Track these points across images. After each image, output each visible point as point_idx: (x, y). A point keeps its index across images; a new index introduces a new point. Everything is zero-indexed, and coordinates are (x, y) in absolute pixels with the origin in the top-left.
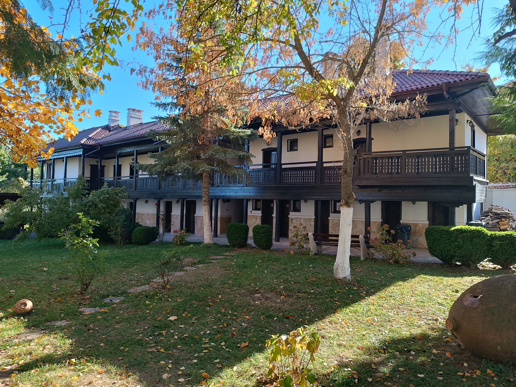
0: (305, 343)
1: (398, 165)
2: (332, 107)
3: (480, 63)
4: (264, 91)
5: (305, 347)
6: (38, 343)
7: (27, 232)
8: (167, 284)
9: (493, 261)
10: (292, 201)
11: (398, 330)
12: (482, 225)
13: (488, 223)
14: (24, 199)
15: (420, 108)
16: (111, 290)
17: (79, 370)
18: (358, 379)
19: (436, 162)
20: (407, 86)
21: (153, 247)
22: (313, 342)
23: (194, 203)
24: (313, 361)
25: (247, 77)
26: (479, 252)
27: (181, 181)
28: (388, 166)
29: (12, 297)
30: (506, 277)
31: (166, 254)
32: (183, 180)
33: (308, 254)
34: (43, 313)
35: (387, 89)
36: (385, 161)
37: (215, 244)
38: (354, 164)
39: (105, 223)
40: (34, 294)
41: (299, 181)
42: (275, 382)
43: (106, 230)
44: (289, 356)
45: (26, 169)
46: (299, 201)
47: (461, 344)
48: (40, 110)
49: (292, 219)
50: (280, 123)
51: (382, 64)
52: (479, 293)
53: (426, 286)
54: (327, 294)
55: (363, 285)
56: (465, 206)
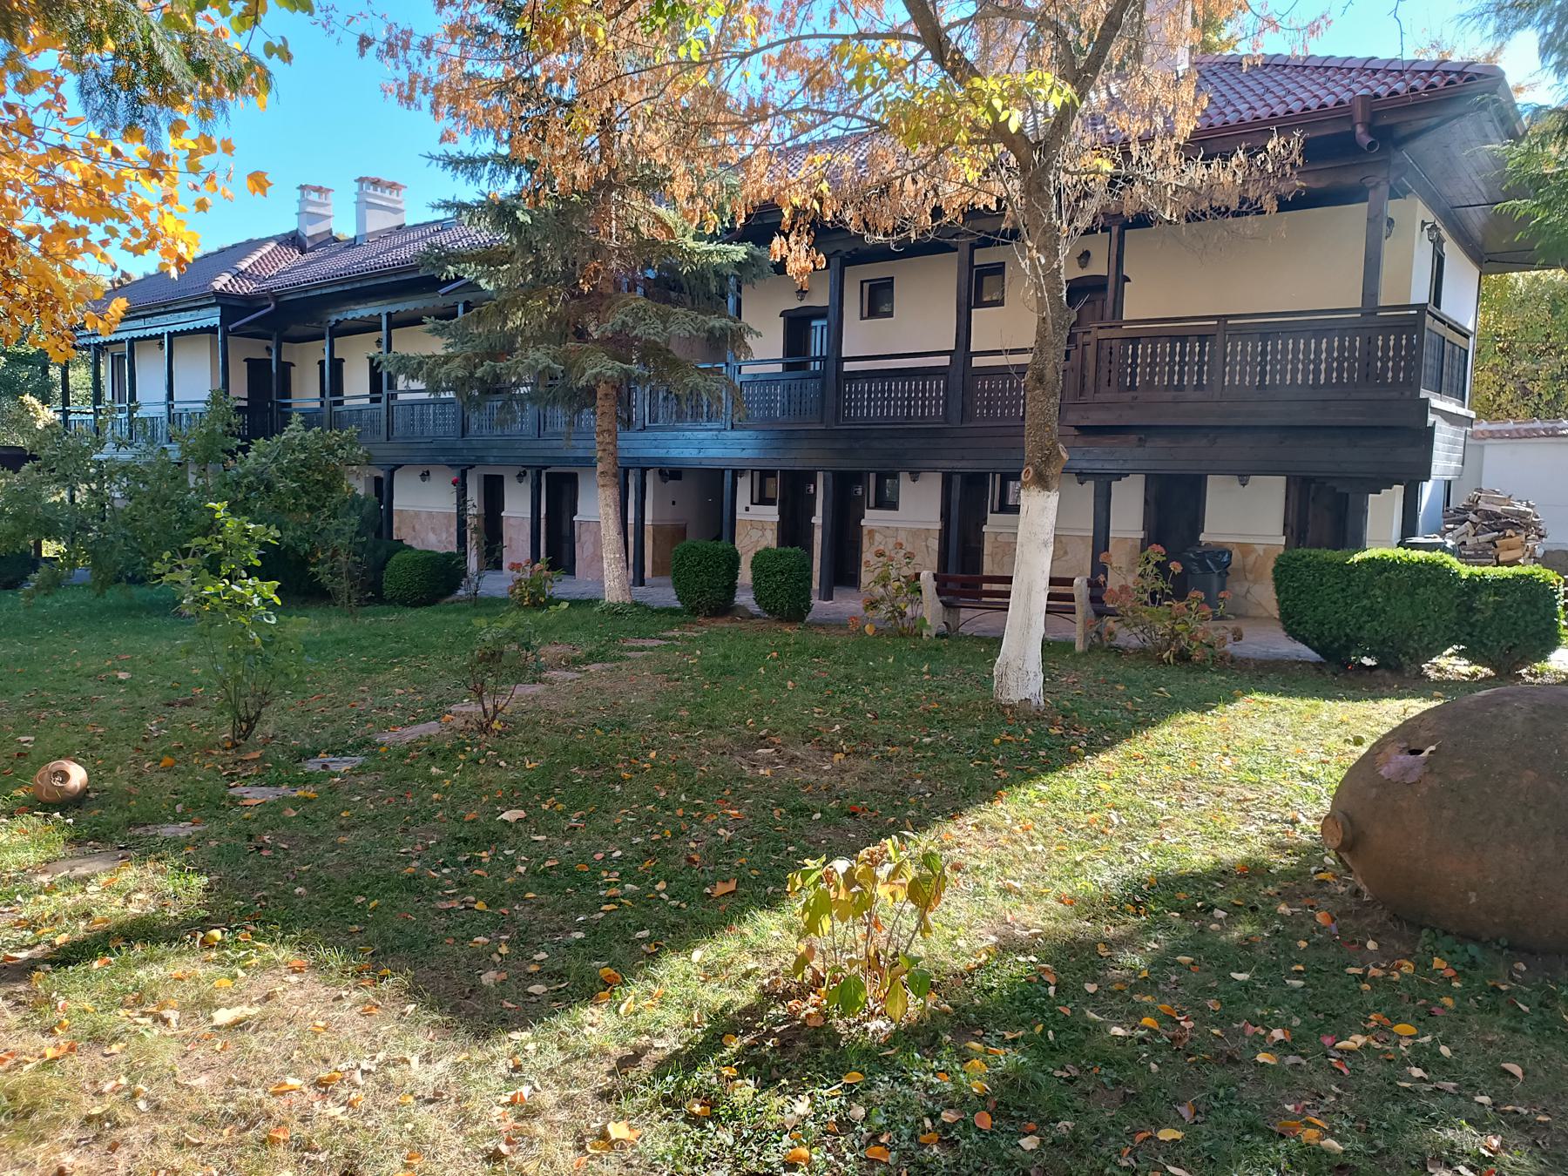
0: (903, 881)
1: (1201, 364)
2: (1003, 172)
3: (1478, 31)
4: (788, 114)
5: (902, 895)
6: (108, 887)
7: (62, 567)
8: (494, 718)
9: (1468, 655)
10: (872, 477)
11: (1180, 850)
12: (1444, 549)
13: (1464, 543)
14: (45, 465)
15: (1279, 180)
16: (325, 735)
17: (233, 962)
18: (1056, 985)
19: (1318, 352)
20: (1243, 107)
21: (448, 612)
22: (926, 880)
23: (573, 479)
24: (927, 934)
25: (733, 67)
26: (1431, 628)
27: (530, 412)
28: (1172, 363)
29: (25, 755)
30: (1510, 695)
31: (488, 630)
32: (536, 407)
33: (917, 635)
34: (122, 799)
35: (1179, 117)
36: (1163, 350)
37: (636, 604)
38: (1067, 358)
39: (301, 539)
40: (92, 748)
41: (895, 412)
42: (815, 992)
43: (303, 562)
44: (854, 917)
45: (45, 370)
46: (895, 476)
47: (1364, 887)
48: (73, 173)
49: (871, 532)
50: (840, 222)
51: (1168, 32)
52: (1425, 742)
53: (1268, 726)
54: (970, 748)
55: (1080, 723)
56: (1399, 490)
